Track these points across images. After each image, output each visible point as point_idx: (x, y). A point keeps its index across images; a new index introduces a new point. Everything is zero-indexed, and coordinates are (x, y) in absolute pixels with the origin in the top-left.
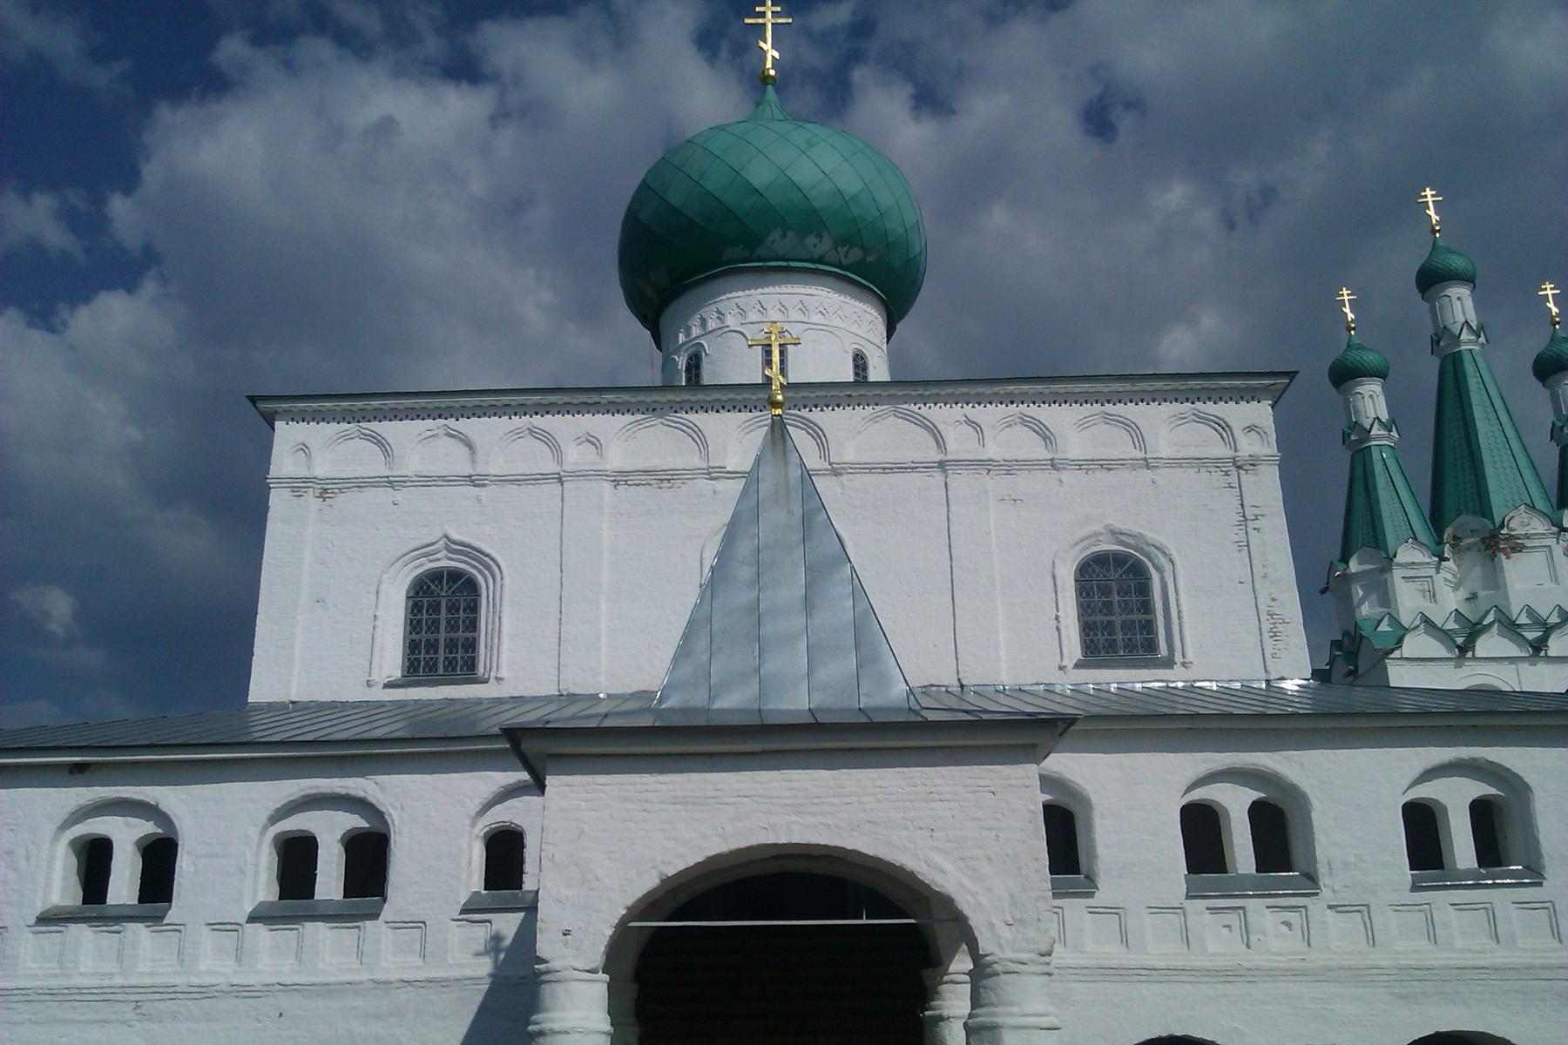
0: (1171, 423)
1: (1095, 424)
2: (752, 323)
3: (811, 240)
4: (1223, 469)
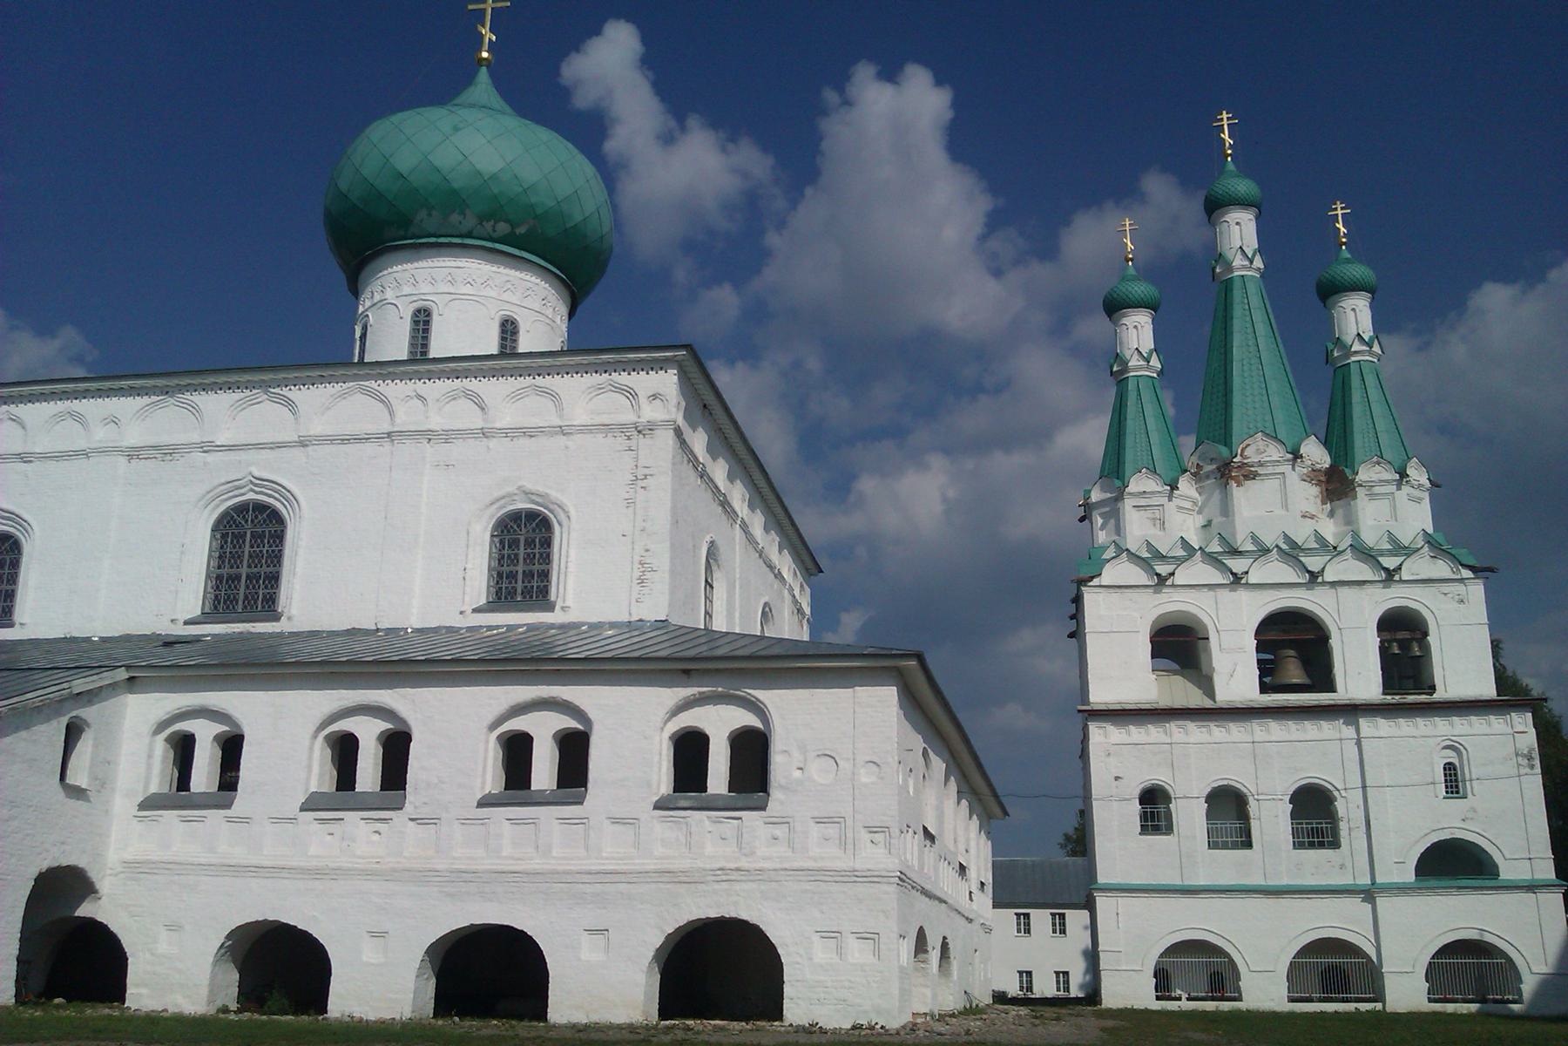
0: (590, 393)
1: (527, 395)
2: (406, 296)
3: (455, 218)
4: (627, 434)
